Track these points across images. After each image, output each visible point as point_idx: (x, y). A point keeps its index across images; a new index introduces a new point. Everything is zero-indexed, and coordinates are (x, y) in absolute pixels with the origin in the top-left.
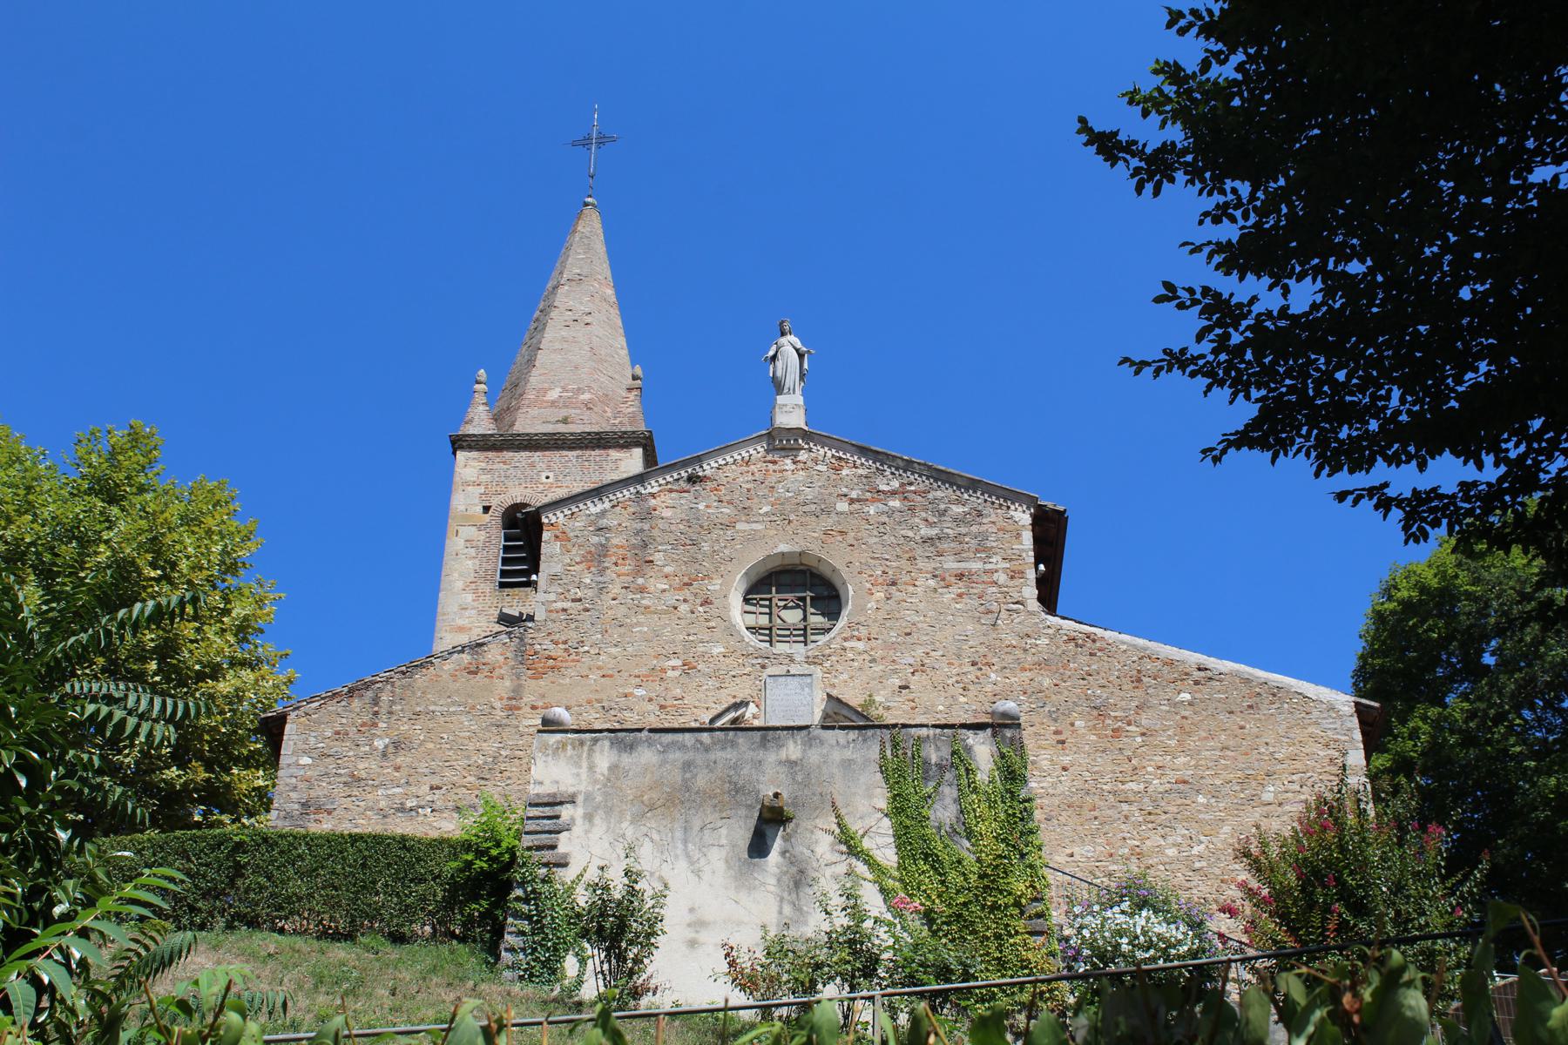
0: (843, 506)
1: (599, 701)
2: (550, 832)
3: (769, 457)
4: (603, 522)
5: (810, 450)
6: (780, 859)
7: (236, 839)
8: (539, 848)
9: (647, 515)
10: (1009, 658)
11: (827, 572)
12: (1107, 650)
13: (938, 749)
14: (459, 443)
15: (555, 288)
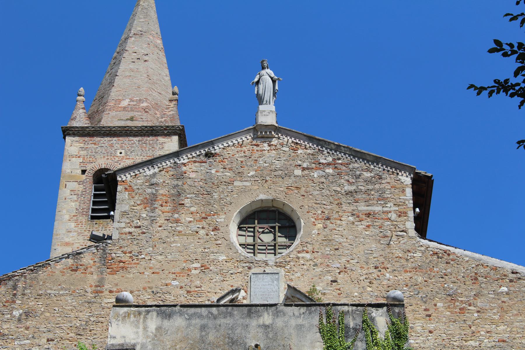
0: (298, 172)
3: (254, 142)
4: (154, 180)
5: (279, 138)
9: (181, 176)
11: (288, 211)
12: (457, 260)
13: (354, 319)
14: (67, 132)
15: (126, 39)
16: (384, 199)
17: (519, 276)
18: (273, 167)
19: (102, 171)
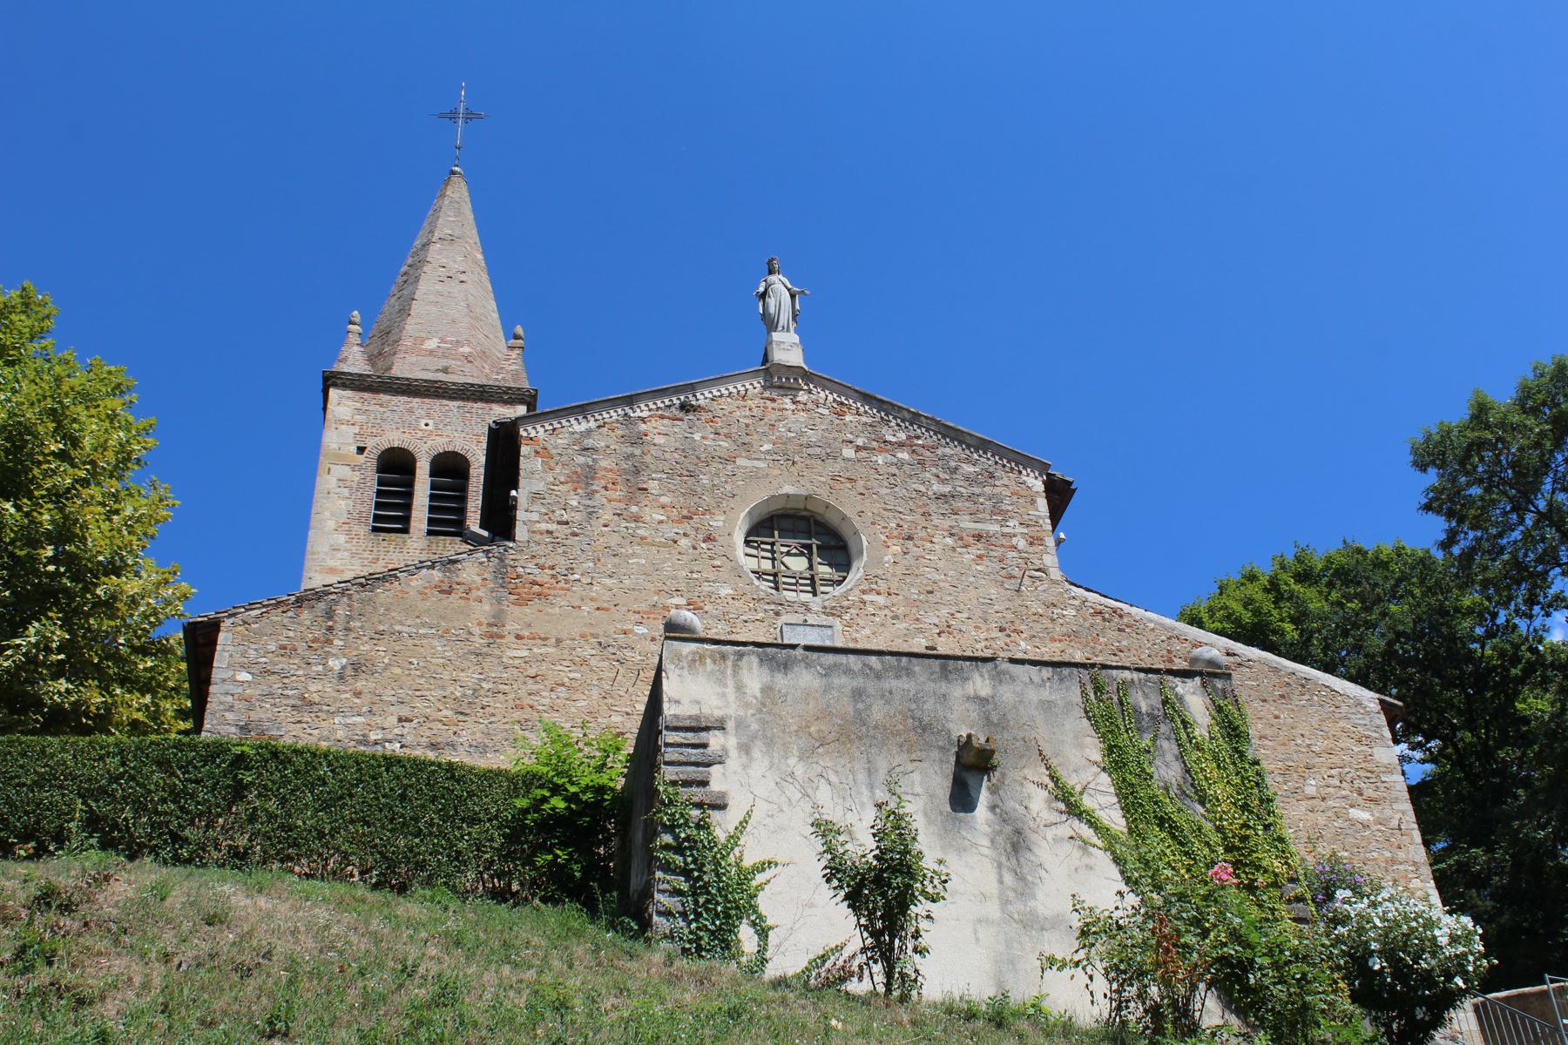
0: (849, 452)
1: (594, 636)
2: (697, 764)
3: (767, 394)
4: (589, 442)
5: (810, 392)
6: (990, 815)
7: (237, 750)
8: (687, 783)
9: (639, 440)
10: (1037, 627)
11: (833, 520)
12: (1135, 626)
13: (1146, 696)
14: (331, 380)
15: (426, 245)
16: (1001, 512)
17: (1238, 660)
18: (804, 440)
19: (391, 450)
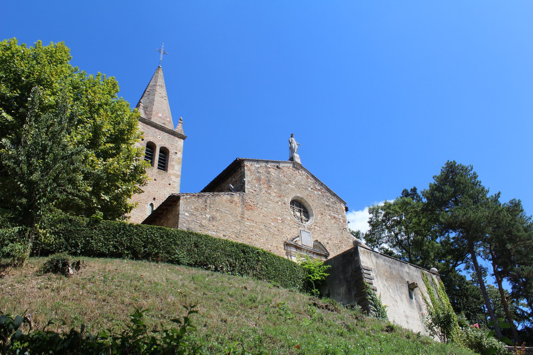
4: (259, 170)
9: (269, 173)
